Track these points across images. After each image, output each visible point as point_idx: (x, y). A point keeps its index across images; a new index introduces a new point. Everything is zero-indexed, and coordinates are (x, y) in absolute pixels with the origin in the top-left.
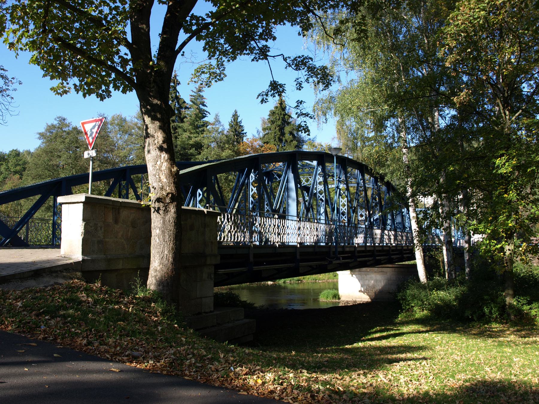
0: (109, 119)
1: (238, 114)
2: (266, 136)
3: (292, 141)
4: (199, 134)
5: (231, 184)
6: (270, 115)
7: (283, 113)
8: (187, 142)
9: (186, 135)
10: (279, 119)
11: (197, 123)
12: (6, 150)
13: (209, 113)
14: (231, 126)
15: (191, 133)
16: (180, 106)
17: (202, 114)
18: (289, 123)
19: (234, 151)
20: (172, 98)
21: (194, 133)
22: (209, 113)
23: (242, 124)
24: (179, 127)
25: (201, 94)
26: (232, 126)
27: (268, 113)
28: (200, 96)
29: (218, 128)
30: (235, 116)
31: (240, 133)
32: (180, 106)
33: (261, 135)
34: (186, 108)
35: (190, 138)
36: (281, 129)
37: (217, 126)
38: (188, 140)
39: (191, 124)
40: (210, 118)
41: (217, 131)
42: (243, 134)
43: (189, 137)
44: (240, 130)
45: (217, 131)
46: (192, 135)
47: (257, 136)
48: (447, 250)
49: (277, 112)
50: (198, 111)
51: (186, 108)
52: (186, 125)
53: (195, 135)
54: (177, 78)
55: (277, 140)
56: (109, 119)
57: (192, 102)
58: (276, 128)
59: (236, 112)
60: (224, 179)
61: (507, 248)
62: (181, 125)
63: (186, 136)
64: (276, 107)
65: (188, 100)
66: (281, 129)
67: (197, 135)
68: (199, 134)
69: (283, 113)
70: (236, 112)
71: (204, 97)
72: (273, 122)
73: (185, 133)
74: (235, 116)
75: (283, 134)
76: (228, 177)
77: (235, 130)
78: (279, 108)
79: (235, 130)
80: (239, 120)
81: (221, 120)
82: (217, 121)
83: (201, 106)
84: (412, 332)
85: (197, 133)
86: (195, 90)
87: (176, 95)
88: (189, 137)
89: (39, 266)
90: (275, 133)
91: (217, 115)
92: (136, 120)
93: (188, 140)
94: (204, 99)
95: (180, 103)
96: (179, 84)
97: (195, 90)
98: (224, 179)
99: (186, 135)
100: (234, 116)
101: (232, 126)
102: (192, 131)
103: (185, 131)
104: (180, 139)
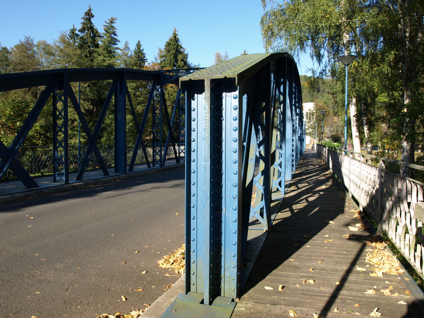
0: (35, 42)
1: (141, 43)
2: (163, 63)
4: (111, 57)
5: (138, 98)
6: (166, 46)
7: (176, 44)
8: (101, 64)
9: (101, 58)
10: (174, 49)
11: (110, 48)
12: (10, 41)
14: (136, 53)
15: (105, 57)
16: (94, 35)
17: (114, 41)
18: (180, 53)
20: (88, 27)
21: (107, 57)
22: (119, 41)
23: (144, 52)
24: (95, 51)
25: (113, 25)
26: (136, 53)
27: (165, 44)
28: (112, 27)
29: (128, 53)
30: (139, 45)
31: (142, 59)
32: (94, 35)
33: (159, 61)
34: (99, 36)
35: (104, 61)
36: (175, 57)
38: (103, 62)
39: (104, 50)
40: (120, 45)
41: (126, 55)
42: (145, 60)
43: (104, 60)
44: (143, 56)
45: (126, 55)
46: (106, 59)
47: (155, 62)
49: (172, 43)
50: (110, 38)
51: (99, 36)
52: (100, 50)
53: (108, 59)
54: (92, 12)
55: (172, 65)
56: (35, 42)
57: (106, 31)
58: (171, 56)
59: (139, 42)
62: (96, 49)
63: (101, 59)
64: (171, 40)
65: (101, 30)
66: (175, 57)
67: (110, 58)
68: (111, 57)
69: (176, 44)
70: (139, 42)
71: (115, 28)
72: (169, 51)
73: (100, 57)
74: (139, 45)
75: (177, 61)
77: (139, 56)
78: (173, 40)
79: (139, 56)
80: (141, 49)
81: (129, 46)
82: (127, 47)
83: (112, 35)
85: (110, 57)
86: (108, 22)
87: (91, 26)
88: (104, 60)
89: (241, 196)
90: (171, 60)
91: (126, 43)
92: (59, 44)
93: (103, 62)
94: (115, 29)
95: (95, 32)
96: (93, 16)
97: (108, 22)
99: (101, 58)
100: (137, 45)
101: (136, 53)
102: (106, 55)
103: (99, 55)
104: (96, 61)
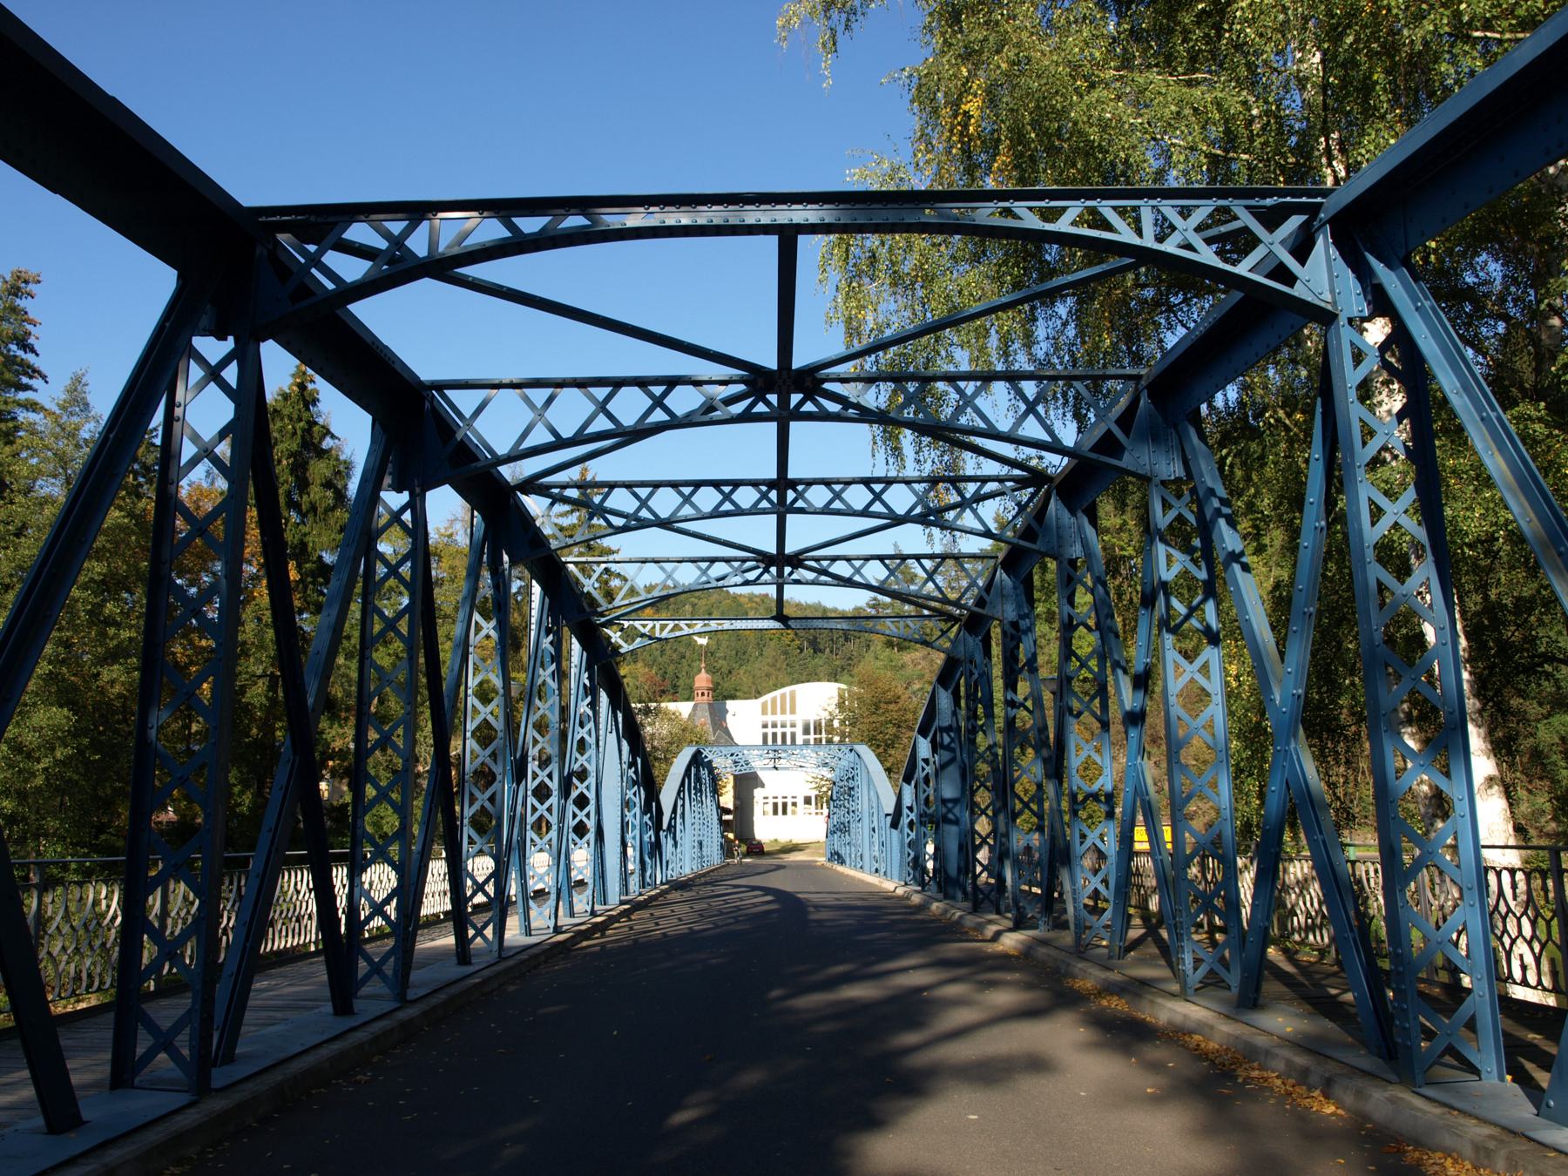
3: (333, 509)
5: (112, 631)
10: (295, 433)
13: (44, 377)
18: (322, 454)
19: (131, 515)
22: (44, 377)
25: (22, 303)
28: (14, 310)
37: (75, 419)
48: (304, 693)
49: (286, 412)
60: (89, 612)
61: (1214, 672)
76: (101, 605)
78: (294, 398)
81: (90, 399)
83: (13, 347)
84: (914, 968)
98: (89, 612)
